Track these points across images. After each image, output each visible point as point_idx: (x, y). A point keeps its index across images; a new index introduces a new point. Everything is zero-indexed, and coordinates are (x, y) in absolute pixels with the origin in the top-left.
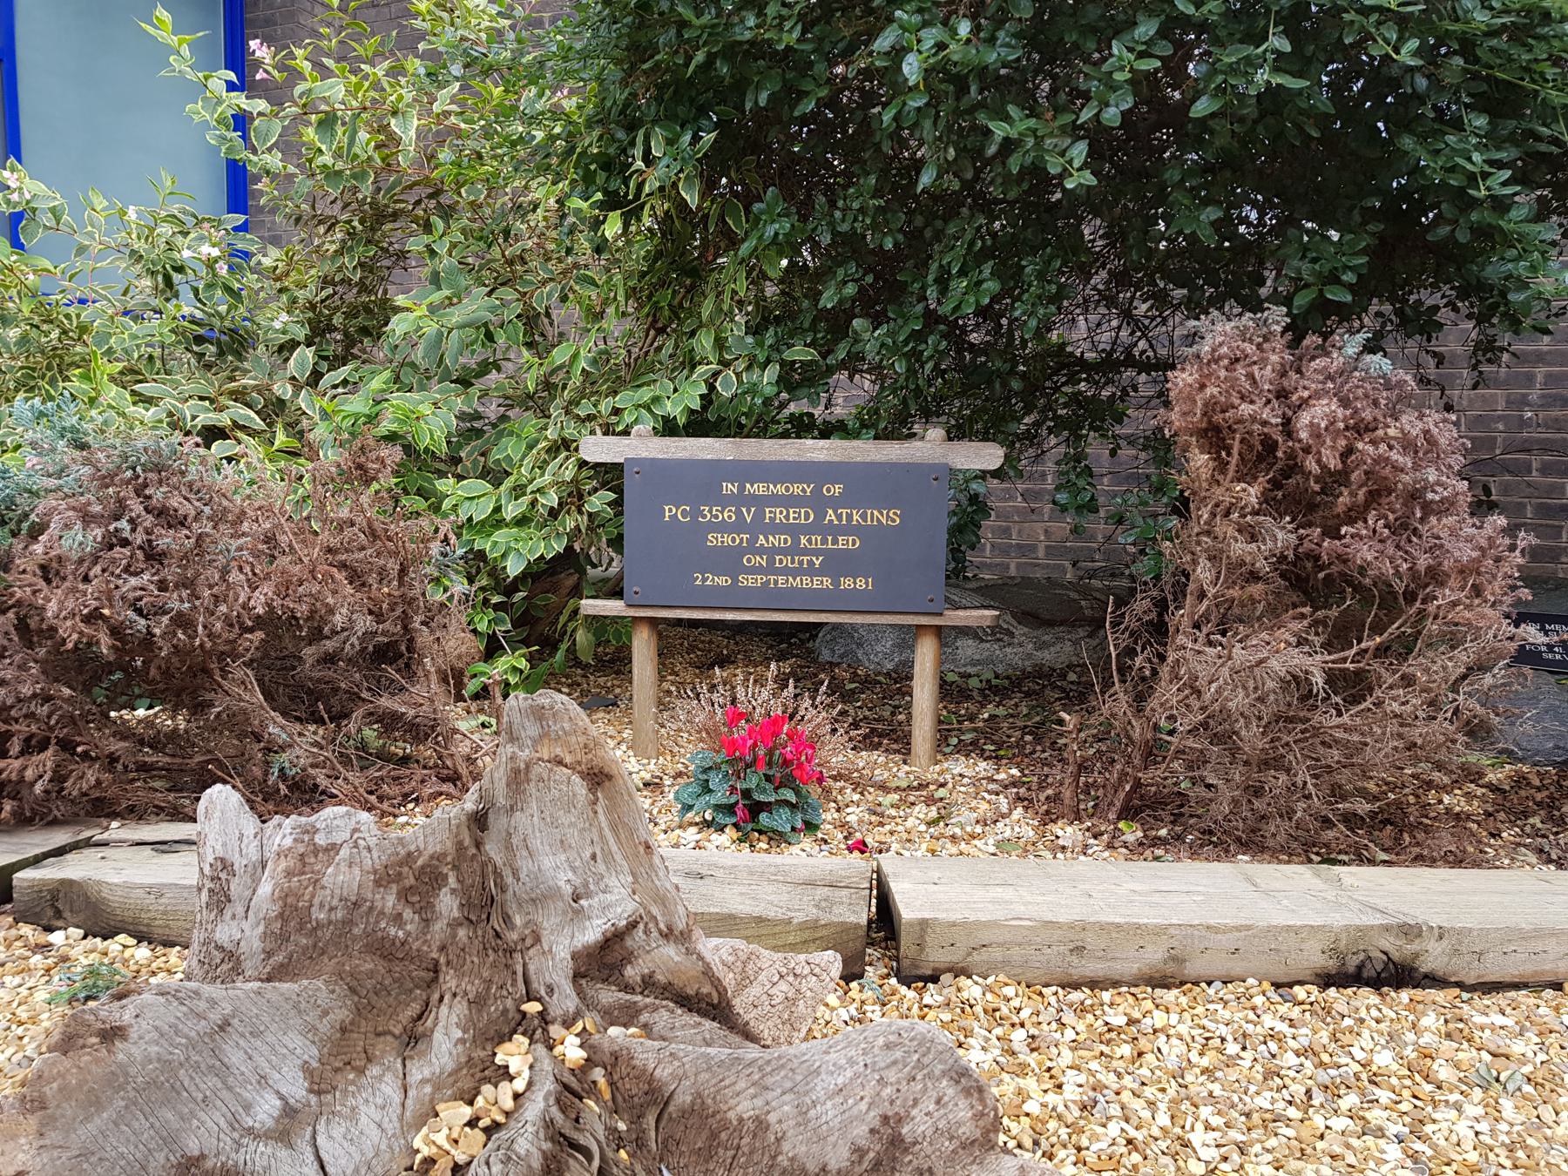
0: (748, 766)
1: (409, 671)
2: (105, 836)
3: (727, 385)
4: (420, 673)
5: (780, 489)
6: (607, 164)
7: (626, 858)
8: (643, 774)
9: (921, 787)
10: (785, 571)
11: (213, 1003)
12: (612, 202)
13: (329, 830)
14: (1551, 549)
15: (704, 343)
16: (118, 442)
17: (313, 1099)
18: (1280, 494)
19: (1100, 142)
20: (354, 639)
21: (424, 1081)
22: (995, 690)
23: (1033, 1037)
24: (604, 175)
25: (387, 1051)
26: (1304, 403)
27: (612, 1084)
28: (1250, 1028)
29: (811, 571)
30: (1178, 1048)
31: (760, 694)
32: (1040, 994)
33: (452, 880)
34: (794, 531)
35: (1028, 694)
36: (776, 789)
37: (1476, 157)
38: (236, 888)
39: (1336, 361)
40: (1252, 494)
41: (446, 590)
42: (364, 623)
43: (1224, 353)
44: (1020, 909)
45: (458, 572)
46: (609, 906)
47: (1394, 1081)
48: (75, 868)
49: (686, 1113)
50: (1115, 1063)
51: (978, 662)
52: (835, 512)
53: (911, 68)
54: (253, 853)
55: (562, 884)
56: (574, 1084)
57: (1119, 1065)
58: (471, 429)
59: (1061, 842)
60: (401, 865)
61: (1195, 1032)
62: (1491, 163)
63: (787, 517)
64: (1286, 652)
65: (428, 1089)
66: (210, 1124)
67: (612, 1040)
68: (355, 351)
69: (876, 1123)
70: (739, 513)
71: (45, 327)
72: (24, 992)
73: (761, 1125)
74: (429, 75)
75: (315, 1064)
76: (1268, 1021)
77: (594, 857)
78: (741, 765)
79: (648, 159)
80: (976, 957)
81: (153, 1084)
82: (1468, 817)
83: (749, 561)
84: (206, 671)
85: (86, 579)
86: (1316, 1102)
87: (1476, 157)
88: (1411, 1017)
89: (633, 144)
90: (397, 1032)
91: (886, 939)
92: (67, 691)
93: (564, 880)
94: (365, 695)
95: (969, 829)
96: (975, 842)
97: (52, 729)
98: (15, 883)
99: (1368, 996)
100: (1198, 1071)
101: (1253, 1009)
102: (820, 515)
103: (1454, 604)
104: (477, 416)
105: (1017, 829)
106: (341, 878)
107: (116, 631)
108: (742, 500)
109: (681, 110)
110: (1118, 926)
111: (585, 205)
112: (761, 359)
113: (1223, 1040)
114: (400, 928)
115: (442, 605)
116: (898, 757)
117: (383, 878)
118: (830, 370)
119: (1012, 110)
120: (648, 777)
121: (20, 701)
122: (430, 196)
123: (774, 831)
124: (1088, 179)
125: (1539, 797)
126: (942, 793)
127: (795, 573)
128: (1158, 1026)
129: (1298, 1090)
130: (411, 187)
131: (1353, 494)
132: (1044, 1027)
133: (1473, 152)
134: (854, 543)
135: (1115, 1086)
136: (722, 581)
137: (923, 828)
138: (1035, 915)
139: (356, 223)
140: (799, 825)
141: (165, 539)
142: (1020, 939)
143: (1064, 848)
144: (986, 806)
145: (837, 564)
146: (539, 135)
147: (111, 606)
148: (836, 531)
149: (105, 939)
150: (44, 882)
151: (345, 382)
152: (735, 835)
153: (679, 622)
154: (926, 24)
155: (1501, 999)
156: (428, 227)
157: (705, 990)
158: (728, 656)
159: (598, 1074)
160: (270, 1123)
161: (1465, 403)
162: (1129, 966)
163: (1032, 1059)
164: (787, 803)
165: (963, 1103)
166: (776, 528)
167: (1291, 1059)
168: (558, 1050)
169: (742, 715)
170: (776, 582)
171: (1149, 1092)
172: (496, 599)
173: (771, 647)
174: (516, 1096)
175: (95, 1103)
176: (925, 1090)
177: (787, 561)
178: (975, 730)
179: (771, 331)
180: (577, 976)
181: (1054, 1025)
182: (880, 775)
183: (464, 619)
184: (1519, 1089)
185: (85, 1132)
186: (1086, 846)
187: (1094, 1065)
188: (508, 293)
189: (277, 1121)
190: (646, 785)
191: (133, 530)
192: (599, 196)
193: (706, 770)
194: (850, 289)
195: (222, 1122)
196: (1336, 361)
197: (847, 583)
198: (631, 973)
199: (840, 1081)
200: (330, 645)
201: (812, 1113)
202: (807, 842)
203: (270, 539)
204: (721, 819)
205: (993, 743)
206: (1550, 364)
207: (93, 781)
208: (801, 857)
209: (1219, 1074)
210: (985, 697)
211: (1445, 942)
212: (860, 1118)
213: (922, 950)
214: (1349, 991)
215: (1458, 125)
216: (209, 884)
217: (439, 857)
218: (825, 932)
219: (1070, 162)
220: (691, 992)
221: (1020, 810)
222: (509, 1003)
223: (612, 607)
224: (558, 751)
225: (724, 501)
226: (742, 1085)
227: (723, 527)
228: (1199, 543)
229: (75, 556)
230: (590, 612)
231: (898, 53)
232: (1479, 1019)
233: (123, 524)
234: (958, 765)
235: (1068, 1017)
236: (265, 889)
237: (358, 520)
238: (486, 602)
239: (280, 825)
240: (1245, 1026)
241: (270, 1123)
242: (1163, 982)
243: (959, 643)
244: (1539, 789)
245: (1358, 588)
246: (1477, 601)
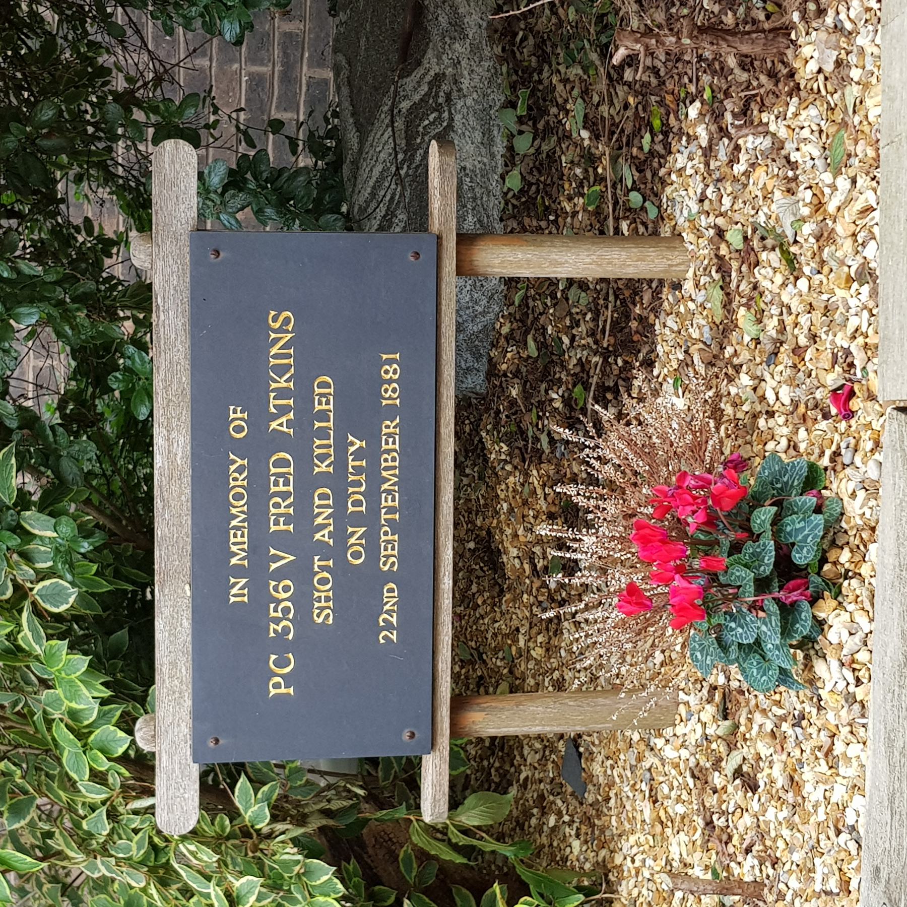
0: (714, 578)
3: (57, 595)
5: (239, 508)
8: (706, 716)
9: (723, 267)
10: (373, 495)
22: (539, 113)
29: (372, 453)
34: (306, 484)
35: (544, 59)
51: (487, 134)
52: (275, 417)
59: (829, 67)
63: (284, 495)
70: (279, 575)
83: (356, 555)
95: (806, 211)
96: (831, 208)
102: (279, 441)
105: (806, 133)
108: (257, 572)
116: (668, 296)
120: (710, 710)
126: (734, 237)
127: (375, 479)
134: (323, 385)
136: (390, 597)
137: (803, 284)
140: (810, 500)
143: (839, 63)
144: (760, 172)
145: (360, 412)
148: (305, 415)
158: (478, 540)
164: (776, 521)
166: (303, 514)
170: (391, 510)
177: (357, 493)
186: (838, 28)
197: (390, 395)
204: (804, 627)
205: (637, 133)
210: (548, 131)
217: (74, 525)
223: (434, 775)
225: (261, 598)
227: (303, 601)
230: (444, 806)
234: (685, 193)
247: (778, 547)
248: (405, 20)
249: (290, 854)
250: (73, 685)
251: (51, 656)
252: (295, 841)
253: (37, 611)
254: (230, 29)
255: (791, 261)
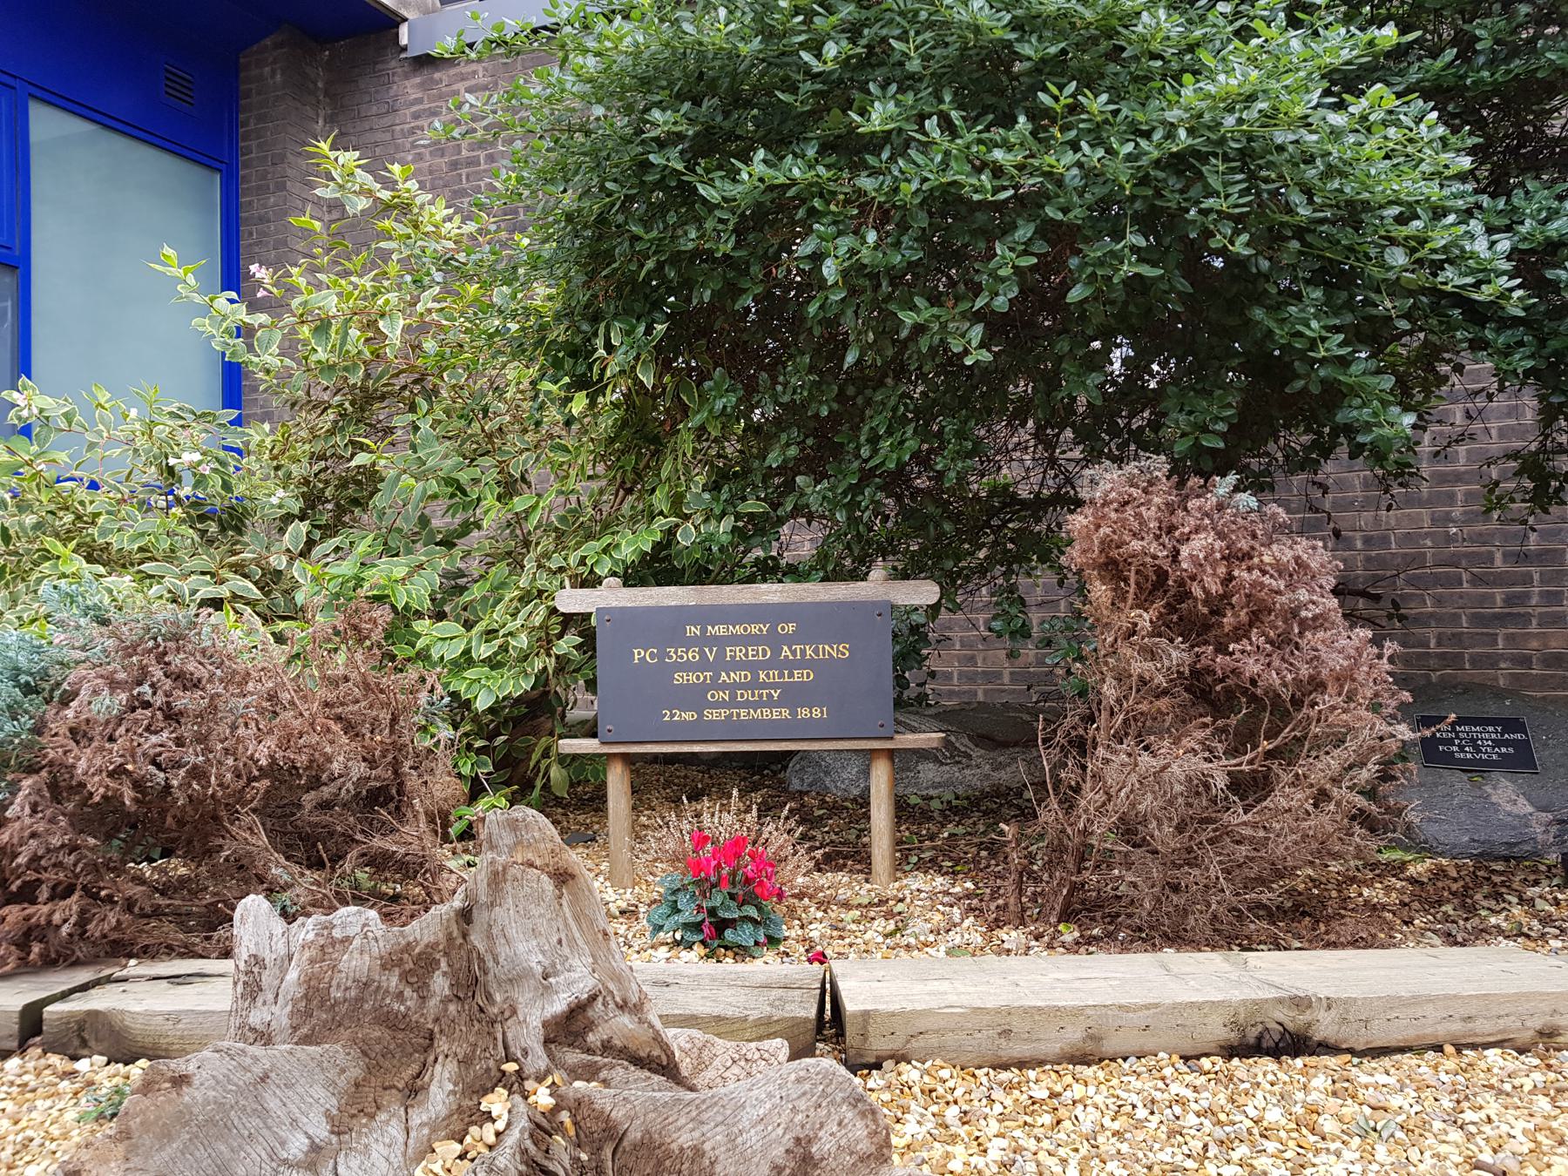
0: (713, 886)
1: (398, 813)
2: (125, 972)
4: (410, 815)
5: (739, 630)
6: (574, 352)
7: (587, 943)
8: (619, 903)
9: (881, 903)
11: (256, 1059)
12: (581, 383)
13: (344, 926)
14: (1488, 656)
15: (660, 500)
16: (141, 616)
17: (334, 1139)
18: (1175, 618)
19: (996, 326)
20: (349, 785)
21: (422, 1125)
22: (954, 811)
23: (965, 1113)
24: (571, 361)
25: (392, 1101)
26: (1186, 539)
27: (575, 1124)
28: (1158, 1095)
29: (770, 703)
30: (1093, 1115)
31: (723, 820)
32: (974, 1075)
33: (443, 964)
34: (753, 667)
35: (985, 813)
36: (739, 907)
37: (1314, 324)
38: (267, 979)
39: (1211, 501)
40: (1145, 619)
41: (433, 736)
42: (359, 769)
43: (1116, 495)
44: (952, 999)
45: (444, 720)
46: (573, 982)
47: (1283, 1134)
48: (100, 1001)
49: (636, 1147)
50: (1036, 1131)
51: (939, 785)
53: (830, 270)
54: (281, 949)
55: (533, 965)
56: (545, 1123)
57: (1038, 1131)
58: (455, 584)
59: (1006, 946)
60: (402, 952)
61: (1109, 1101)
62: (1328, 328)
63: (746, 655)
64: (1189, 759)
65: (426, 1131)
66: (254, 1155)
67: (576, 1090)
68: (346, 519)
69: (791, 1144)
71: (61, 514)
72: (54, 1113)
73: (698, 1152)
74: (415, 282)
75: (335, 1112)
76: (1175, 1088)
77: (560, 942)
78: (707, 885)
79: (609, 348)
80: (914, 1044)
81: (210, 1121)
82: (1384, 907)
84: (216, 818)
85: (111, 739)
86: (1210, 1154)
87: (1314, 324)
88: (1303, 1080)
89: (596, 334)
90: (400, 1086)
91: (837, 1035)
92: (92, 841)
93: (535, 961)
94: (359, 837)
95: (922, 938)
97: (77, 876)
98: (45, 1016)
99: (1268, 1064)
100: (1109, 1134)
101: (1163, 1079)
102: (777, 651)
103: (1333, 708)
104: (461, 574)
106: (355, 963)
107: (138, 785)
108: (704, 641)
109: (638, 307)
110: (1039, 1009)
111: (554, 388)
112: (717, 512)
113: (1134, 1107)
114: (402, 1003)
115: (430, 751)
116: (861, 877)
117: (387, 964)
118: (781, 521)
119: (918, 301)
120: (624, 905)
121: (48, 851)
122: (415, 382)
123: (739, 946)
124: (985, 356)
125: (1454, 887)
126: (900, 907)
127: (756, 706)
128: (1077, 1097)
129: (1197, 1146)
130: (397, 375)
131: (1235, 615)
132: (976, 1103)
133: (1310, 320)
135: (1034, 1149)
136: (688, 716)
137: (880, 939)
138: (966, 1003)
139: (347, 405)
140: (762, 939)
141: (183, 700)
142: (953, 1026)
143: (1009, 951)
144: (940, 917)
145: (793, 696)
146: (514, 326)
147: (135, 762)
148: (791, 665)
149: (126, 1064)
150: (71, 1014)
151: (337, 549)
152: (703, 951)
153: (655, 758)
154: (840, 234)
155: (1386, 1062)
156: (413, 408)
157: (656, 1053)
158: (703, 789)
159: (565, 1116)
160: (301, 1156)
161: (1393, 523)
162: (1052, 1045)
163: (962, 1131)
165: (860, 1124)
166: (736, 665)
167: (1192, 1120)
168: (532, 1099)
169: (707, 838)
170: (738, 715)
171: (1062, 1152)
172: (479, 744)
173: (744, 779)
174: (498, 1134)
175: (166, 1136)
176: (829, 1114)
177: (748, 695)
178: (934, 848)
179: (726, 488)
180: (547, 1041)
181: (984, 1101)
182: (844, 893)
183: (449, 763)
184: (1392, 1136)
185: (161, 1158)
186: (1029, 948)
187: (1018, 1133)
188: (486, 461)
189: (306, 1154)
190: (622, 913)
191: (154, 693)
192: (567, 379)
193: (675, 892)
194: (793, 451)
195: (264, 1156)
196: (1211, 501)
197: (803, 713)
198: (593, 1038)
199: (761, 1112)
200: (326, 792)
201: (739, 1140)
202: (770, 955)
203: (272, 697)
204: (690, 937)
205: (951, 859)
206: (1467, 483)
207: (114, 921)
208: (766, 966)
209: (1128, 1135)
210: (945, 817)
211: (1333, 1012)
212: (778, 1141)
213: (866, 1040)
214: (1251, 1061)
215: (1298, 297)
216: (243, 978)
217: (433, 946)
218: (777, 1028)
219: (969, 342)
220: (643, 1054)
221: (971, 919)
222: (491, 1063)
224: (530, 856)
225: (689, 643)
226: (682, 1121)
227: (688, 667)
228: (1106, 664)
229: (102, 718)
230: (567, 751)
231: (817, 258)
232: (1364, 1079)
233: (146, 688)
234: (918, 882)
235: (998, 1094)
236: (293, 975)
237: (354, 675)
238: (469, 747)
239: (303, 925)
240: (1154, 1093)
241: (301, 1156)
242: (1085, 1059)
243: (920, 767)
244: (1455, 880)
245: (1254, 698)
246: (1352, 705)
247: (734, 920)
248: (1000, 737)
249: (538, 664)
250: (632, 544)
251: (652, 532)
252: (545, 668)
253: (677, 526)
254: (997, 625)
255: (891, 934)
